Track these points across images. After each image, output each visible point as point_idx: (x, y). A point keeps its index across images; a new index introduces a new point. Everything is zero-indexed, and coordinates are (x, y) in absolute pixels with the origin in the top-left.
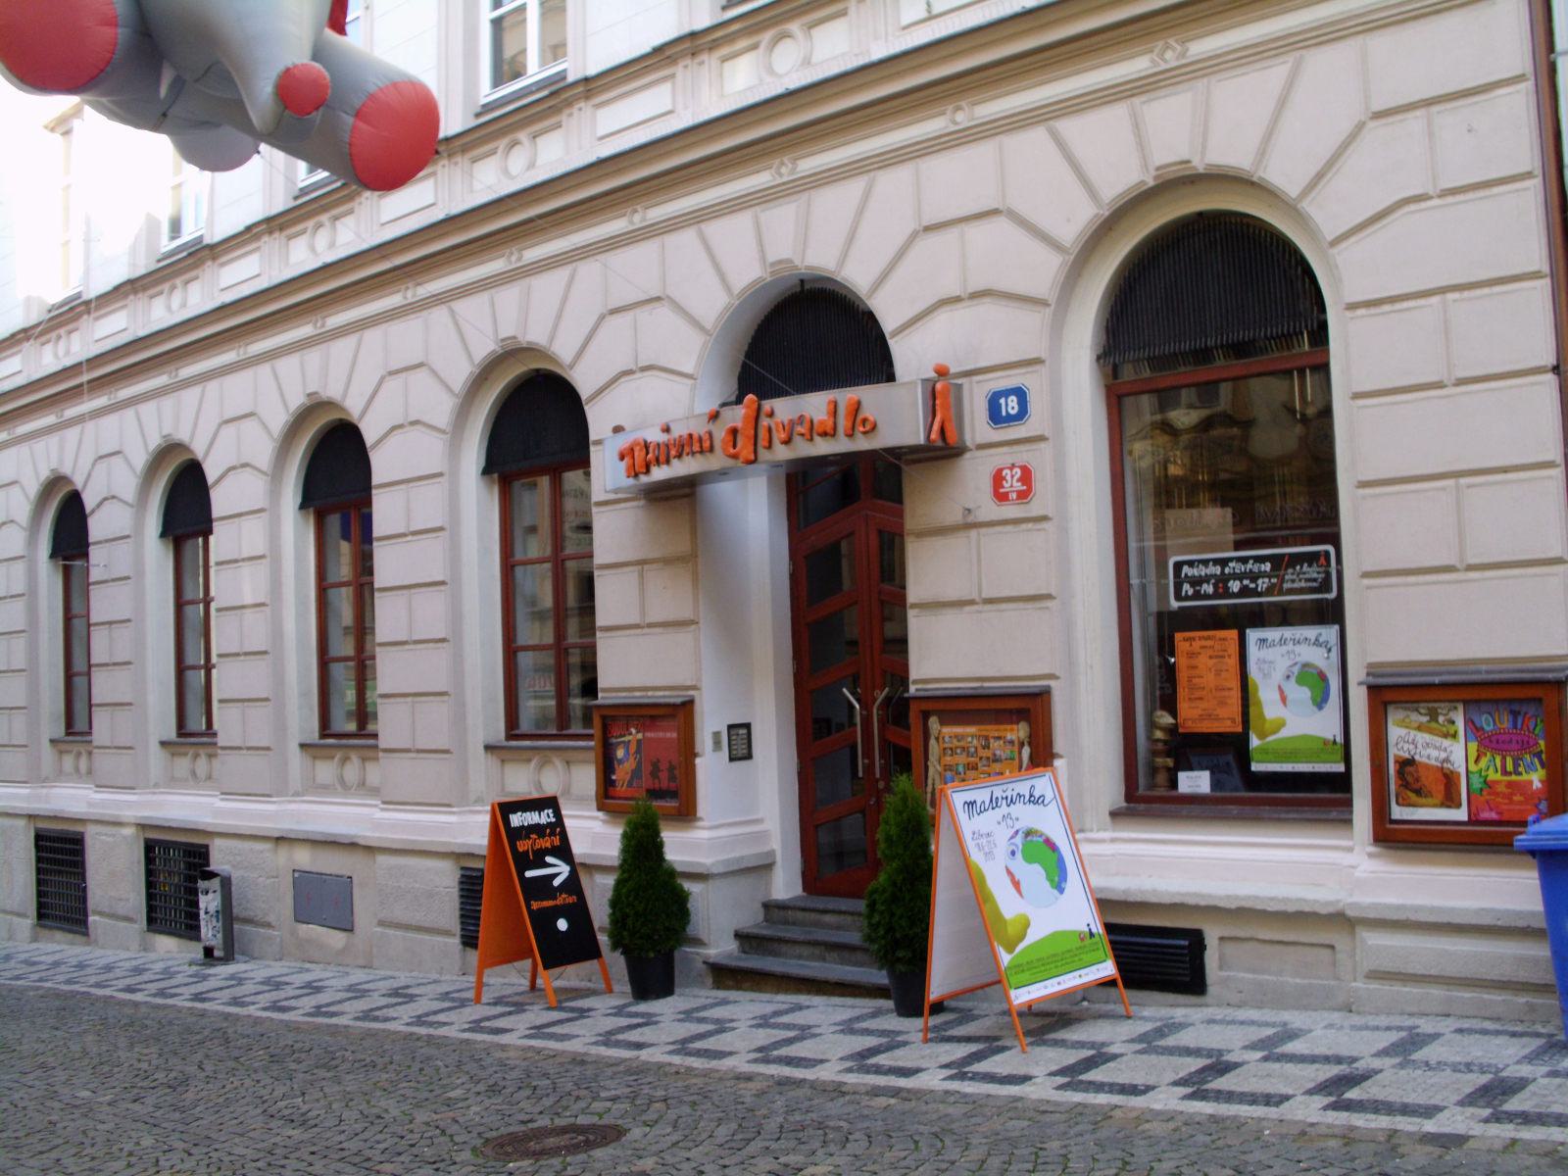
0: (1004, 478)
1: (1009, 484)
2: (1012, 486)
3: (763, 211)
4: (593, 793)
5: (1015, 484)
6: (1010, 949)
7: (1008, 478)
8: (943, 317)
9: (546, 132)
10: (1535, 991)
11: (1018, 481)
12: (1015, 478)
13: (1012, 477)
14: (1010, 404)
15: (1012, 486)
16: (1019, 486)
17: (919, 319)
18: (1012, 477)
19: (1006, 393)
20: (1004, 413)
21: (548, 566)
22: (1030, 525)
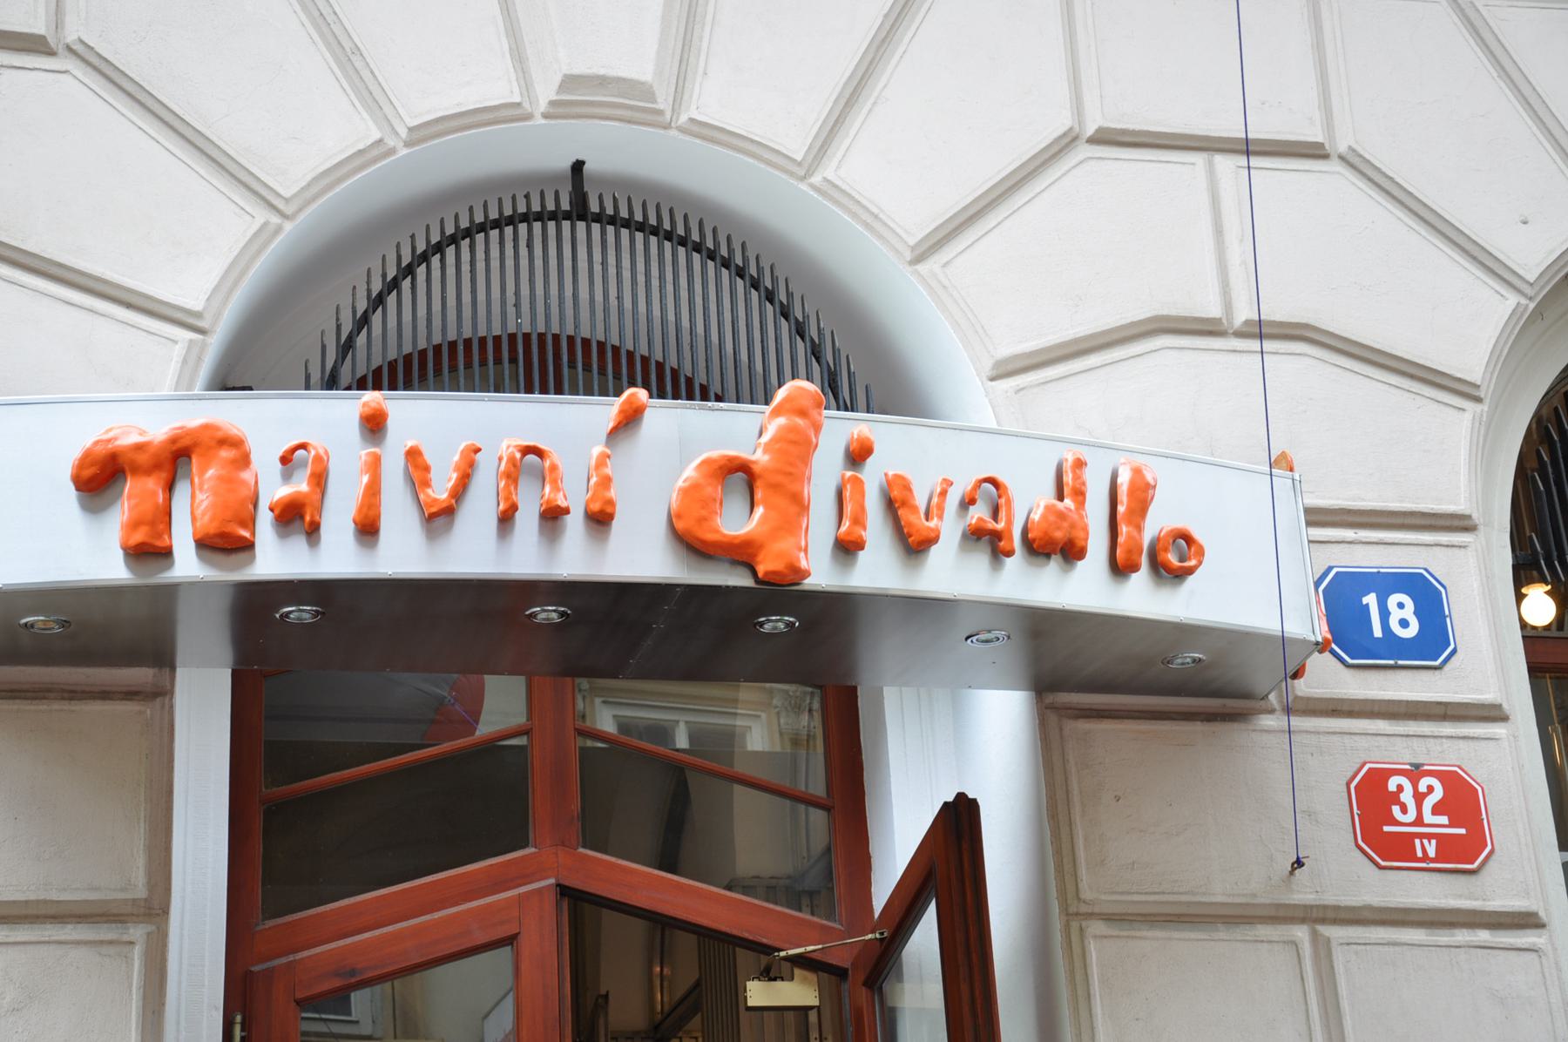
0: (1395, 798)
1: (1411, 816)
2: (1419, 821)
3: (873, 221)
4: (463, 265)
5: (1428, 817)
6: (794, 624)
7: (1407, 797)
8: (1168, 354)
9: (1128, 718)
10: (123, 699)
11: (1436, 810)
12: (1428, 804)
13: (1419, 798)
14: (1395, 616)
15: (1419, 821)
16: (1439, 823)
17: (1340, 660)
18: (1419, 798)
19: (1388, 583)
20: (1378, 632)
21: (903, 689)
22: (1484, 936)
